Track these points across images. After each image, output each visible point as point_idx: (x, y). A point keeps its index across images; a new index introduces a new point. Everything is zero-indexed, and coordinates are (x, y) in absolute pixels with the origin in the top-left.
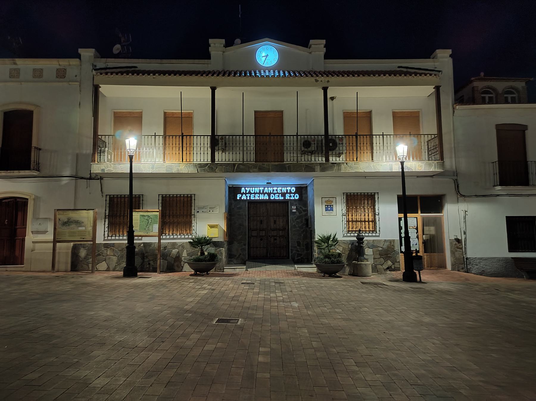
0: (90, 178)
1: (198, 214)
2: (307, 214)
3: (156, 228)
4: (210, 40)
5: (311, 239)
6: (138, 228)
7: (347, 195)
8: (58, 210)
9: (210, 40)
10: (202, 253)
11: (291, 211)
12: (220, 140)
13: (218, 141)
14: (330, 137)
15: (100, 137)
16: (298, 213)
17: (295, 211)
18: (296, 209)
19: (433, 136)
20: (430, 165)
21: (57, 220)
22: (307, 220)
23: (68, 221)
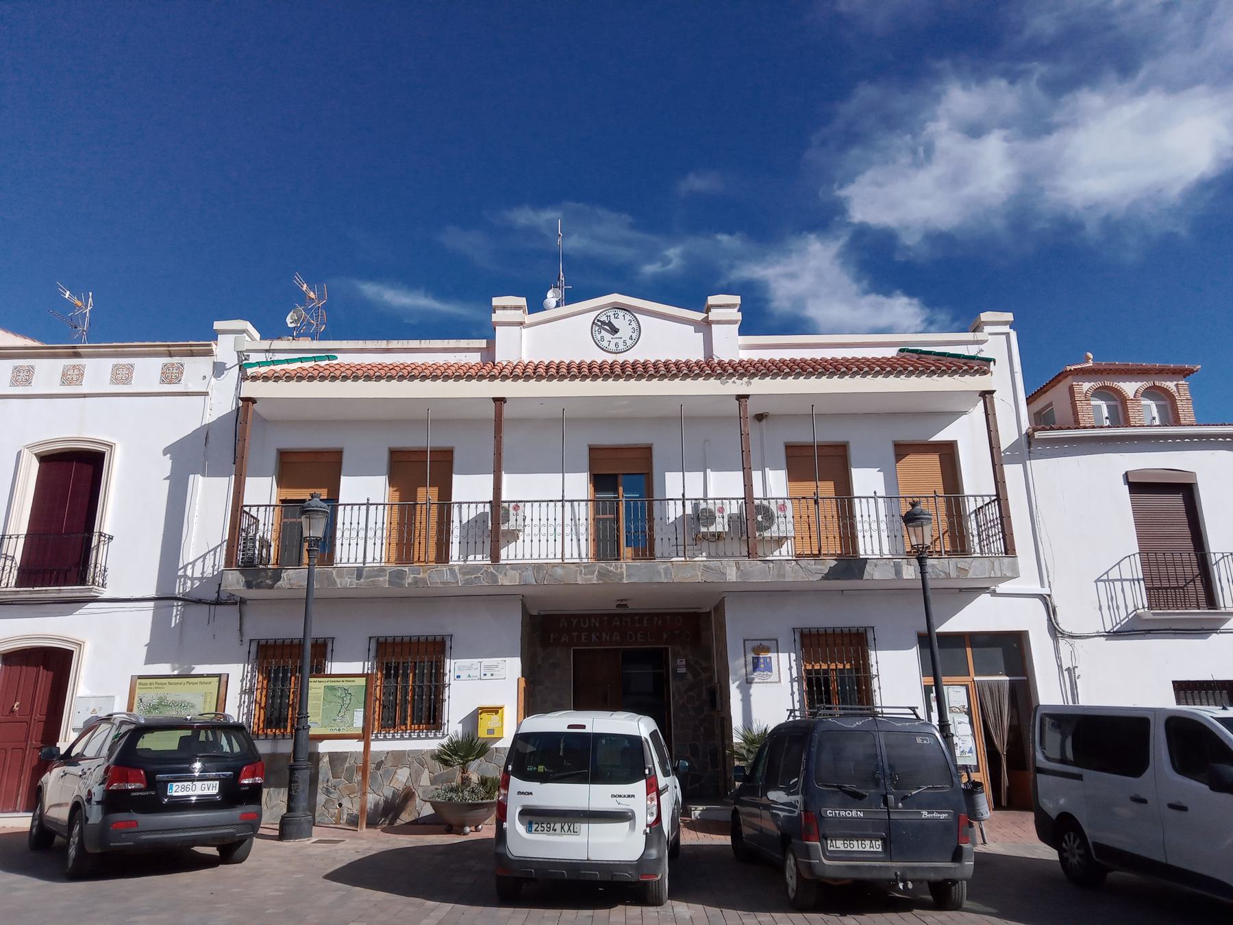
0: (218, 602)
1: (458, 682)
2: (711, 679)
3: (358, 721)
4: (832, 483)
5: (723, 741)
6: (318, 719)
7: (803, 635)
8: (140, 677)
9: (832, 483)
10: (465, 781)
11: (675, 670)
12: (512, 511)
13: (507, 511)
14: (757, 502)
15: (247, 509)
16: (690, 676)
17: (682, 670)
18: (688, 666)
19: (987, 500)
20: (837, 238)
21: (136, 700)
22: (712, 693)
23: (160, 704)
